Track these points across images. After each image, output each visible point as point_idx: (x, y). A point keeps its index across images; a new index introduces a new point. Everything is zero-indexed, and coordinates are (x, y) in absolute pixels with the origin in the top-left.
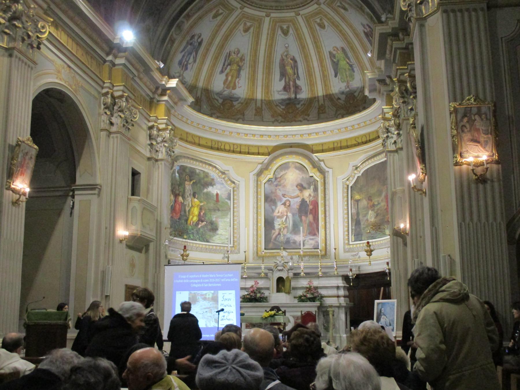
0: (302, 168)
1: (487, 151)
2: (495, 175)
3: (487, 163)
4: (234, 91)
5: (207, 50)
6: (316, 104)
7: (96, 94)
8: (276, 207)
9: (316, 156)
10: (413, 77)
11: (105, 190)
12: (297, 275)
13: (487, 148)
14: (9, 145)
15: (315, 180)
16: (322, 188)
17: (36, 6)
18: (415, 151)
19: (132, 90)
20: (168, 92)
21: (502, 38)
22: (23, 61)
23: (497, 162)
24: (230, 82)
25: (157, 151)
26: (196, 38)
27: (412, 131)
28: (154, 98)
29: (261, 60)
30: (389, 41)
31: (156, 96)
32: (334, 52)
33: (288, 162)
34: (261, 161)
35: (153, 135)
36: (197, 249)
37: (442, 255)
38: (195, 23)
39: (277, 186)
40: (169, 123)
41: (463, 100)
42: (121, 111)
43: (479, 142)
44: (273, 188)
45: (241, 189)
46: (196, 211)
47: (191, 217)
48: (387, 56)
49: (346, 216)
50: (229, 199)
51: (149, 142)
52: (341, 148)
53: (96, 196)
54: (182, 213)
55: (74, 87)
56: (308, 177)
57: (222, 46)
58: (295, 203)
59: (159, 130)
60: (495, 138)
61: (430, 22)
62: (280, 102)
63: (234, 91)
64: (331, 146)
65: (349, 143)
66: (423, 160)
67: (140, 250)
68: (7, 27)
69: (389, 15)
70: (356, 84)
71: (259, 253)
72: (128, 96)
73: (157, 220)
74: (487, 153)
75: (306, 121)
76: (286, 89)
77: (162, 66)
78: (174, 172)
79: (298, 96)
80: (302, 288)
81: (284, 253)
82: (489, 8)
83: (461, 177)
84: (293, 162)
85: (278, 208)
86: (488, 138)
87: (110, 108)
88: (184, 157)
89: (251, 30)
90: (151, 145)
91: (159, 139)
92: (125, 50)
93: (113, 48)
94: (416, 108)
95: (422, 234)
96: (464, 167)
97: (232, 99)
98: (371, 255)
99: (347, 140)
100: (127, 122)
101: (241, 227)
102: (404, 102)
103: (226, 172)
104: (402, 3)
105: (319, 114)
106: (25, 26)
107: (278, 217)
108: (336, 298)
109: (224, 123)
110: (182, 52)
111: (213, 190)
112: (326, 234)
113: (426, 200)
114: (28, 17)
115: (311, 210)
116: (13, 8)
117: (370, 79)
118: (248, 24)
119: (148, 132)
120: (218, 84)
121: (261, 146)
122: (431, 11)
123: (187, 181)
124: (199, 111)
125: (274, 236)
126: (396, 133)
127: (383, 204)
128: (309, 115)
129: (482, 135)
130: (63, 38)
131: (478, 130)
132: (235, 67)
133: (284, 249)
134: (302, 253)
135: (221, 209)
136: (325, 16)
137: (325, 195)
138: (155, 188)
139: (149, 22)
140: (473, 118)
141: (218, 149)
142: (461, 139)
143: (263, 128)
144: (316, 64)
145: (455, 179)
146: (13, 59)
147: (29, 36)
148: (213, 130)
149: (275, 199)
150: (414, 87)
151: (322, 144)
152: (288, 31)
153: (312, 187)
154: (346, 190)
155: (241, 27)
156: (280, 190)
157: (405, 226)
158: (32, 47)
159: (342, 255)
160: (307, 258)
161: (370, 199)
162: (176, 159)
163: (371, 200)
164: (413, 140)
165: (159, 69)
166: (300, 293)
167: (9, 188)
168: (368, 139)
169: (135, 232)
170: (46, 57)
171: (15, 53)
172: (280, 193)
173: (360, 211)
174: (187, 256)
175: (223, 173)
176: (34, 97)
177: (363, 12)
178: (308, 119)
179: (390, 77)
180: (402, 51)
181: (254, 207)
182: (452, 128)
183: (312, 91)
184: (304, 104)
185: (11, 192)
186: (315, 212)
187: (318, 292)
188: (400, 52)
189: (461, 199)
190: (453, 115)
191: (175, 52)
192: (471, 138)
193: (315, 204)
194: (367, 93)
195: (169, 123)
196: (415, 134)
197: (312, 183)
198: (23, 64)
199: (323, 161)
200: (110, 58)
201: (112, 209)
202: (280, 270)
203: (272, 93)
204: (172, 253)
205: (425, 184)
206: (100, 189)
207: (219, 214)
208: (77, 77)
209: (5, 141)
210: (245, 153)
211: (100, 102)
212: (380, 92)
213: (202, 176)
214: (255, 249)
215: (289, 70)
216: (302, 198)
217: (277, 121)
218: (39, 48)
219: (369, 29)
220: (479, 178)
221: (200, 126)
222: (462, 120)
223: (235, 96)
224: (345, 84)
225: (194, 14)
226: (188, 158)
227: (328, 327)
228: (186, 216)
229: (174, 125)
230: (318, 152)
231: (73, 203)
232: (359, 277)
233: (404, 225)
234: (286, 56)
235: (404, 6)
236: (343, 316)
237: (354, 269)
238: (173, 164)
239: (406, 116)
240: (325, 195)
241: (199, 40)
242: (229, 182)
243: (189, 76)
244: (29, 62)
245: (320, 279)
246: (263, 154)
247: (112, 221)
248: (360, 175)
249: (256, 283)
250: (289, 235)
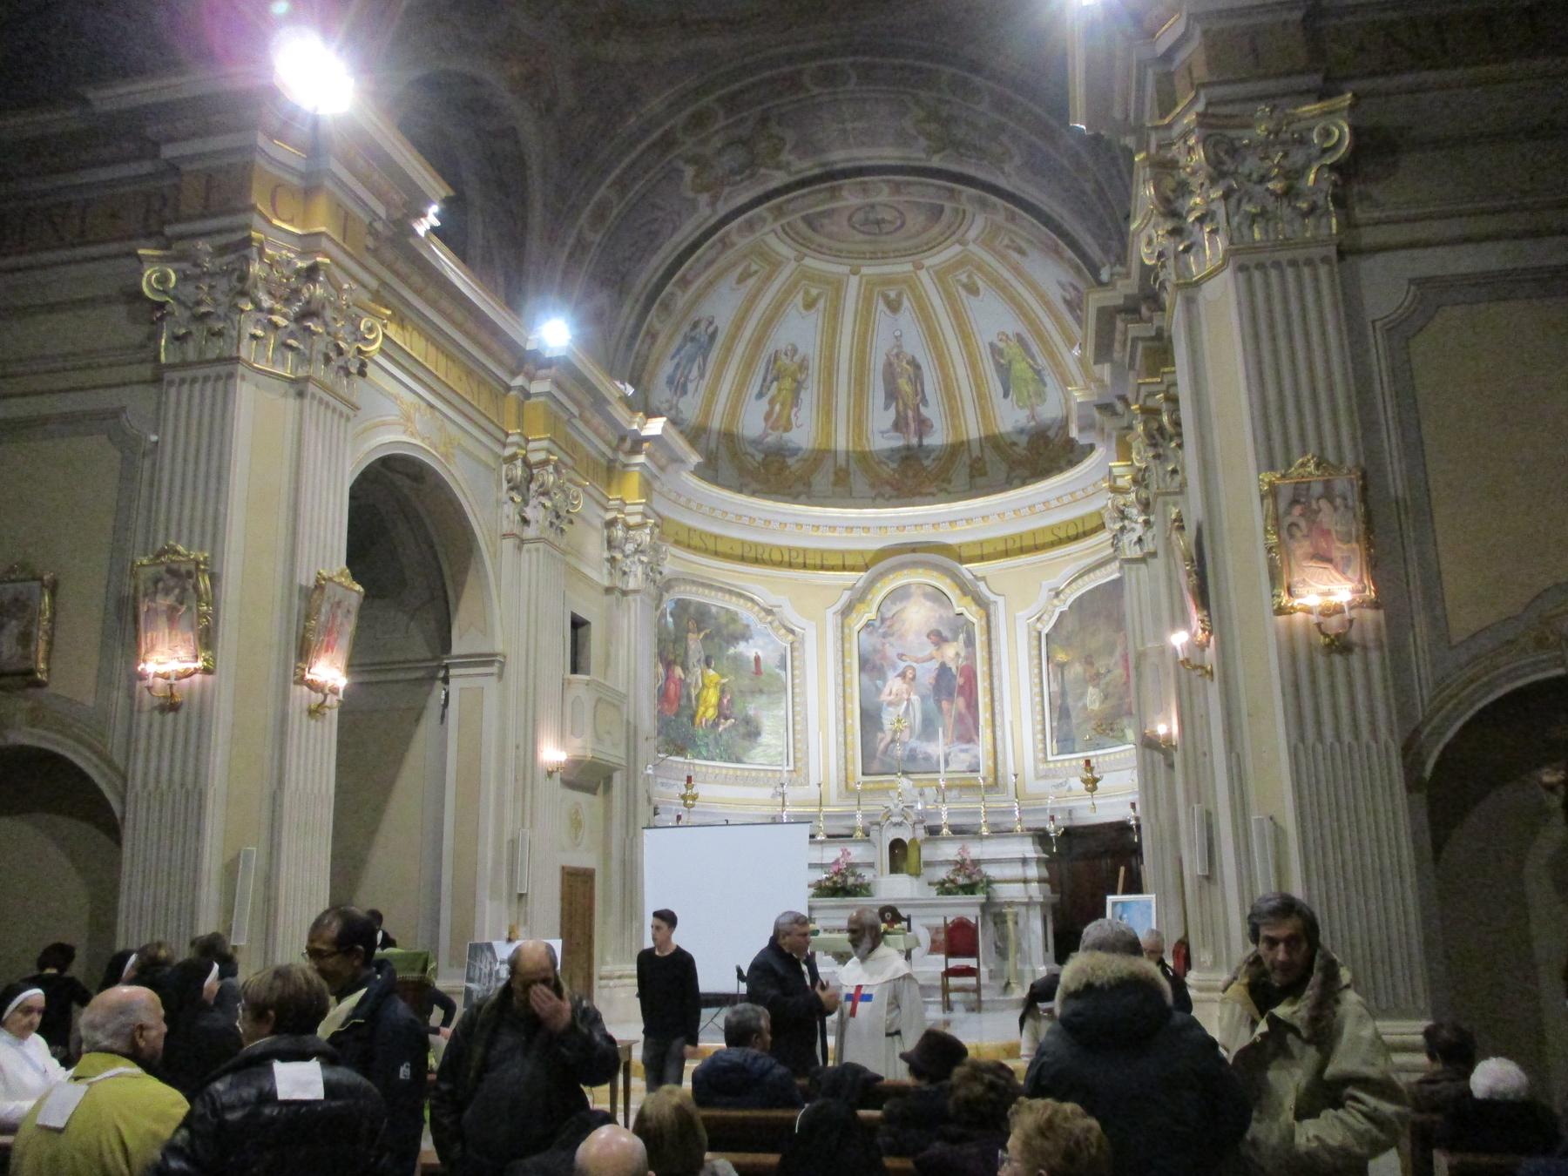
0: (938, 596)
1: (1349, 579)
2: (1371, 635)
3: (1351, 608)
4: (786, 436)
5: (728, 350)
6: (966, 458)
7: (491, 462)
8: (885, 680)
10: (1173, 400)
11: (513, 668)
12: (933, 831)
13: (1350, 574)
14: (301, 588)
15: (968, 622)
16: (984, 638)
17: (354, 286)
18: (1183, 579)
19: (571, 448)
20: (646, 445)
21: (1373, 322)
22: (327, 405)
23: (1376, 605)
24: (780, 415)
25: (625, 573)
26: (703, 326)
27: (1175, 535)
28: (614, 461)
29: (844, 366)
30: (1120, 325)
31: (621, 457)
32: (1001, 345)
33: (909, 585)
34: (850, 583)
36: (717, 780)
37: (1254, 817)
38: (699, 297)
39: (885, 635)
40: (649, 512)
41: (1290, 466)
42: (546, 494)
43: (1330, 561)
44: (875, 640)
45: (807, 646)
46: (712, 696)
47: (702, 709)
48: (1116, 356)
49: (1038, 699)
51: (606, 555)
52: (1023, 551)
53: (494, 679)
54: (684, 702)
55: (442, 449)
56: (951, 615)
57: (758, 342)
58: (927, 673)
59: (628, 527)
60: (1368, 549)
61: (1210, 290)
63: (786, 436)
64: (1001, 547)
65: (1040, 541)
66: (1202, 597)
67: (592, 790)
68: (292, 335)
69: (1118, 269)
70: (1050, 411)
71: (851, 783)
72: (560, 460)
73: (628, 722)
74: (1350, 586)
75: (943, 495)
76: (899, 425)
77: (630, 391)
78: (663, 615)
80: (948, 862)
81: (904, 783)
82: (1342, 254)
83: (1291, 638)
84: (920, 585)
85: (890, 683)
86: (1353, 550)
87: (520, 487)
89: (821, 304)
90: (612, 560)
92: (549, 364)
93: (525, 361)
94: (1183, 469)
95: (1206, 749)
96: (1299, 616)
98: (1094, 788)
99: (1034, 533)
100: (558, 517)
101: (808, 735)
102: (1157, 457)
104: (1144, 250)
105: (972, 477)
106: (331, 330)
107: (890, 704)
108: (1021, 885)
109: (768, 504)
110: (673, 357)
111: (747, 650)
112: (994, 739)
113: (1214, 689)
114: (338, 309)
115: (961, 687)
116: (306, 294)
117: (1081, 404)
118: (814, 292)
120: (753, 422)
121: (850, 552)
122: (1209, 267)
123: (690, 633)
124: (714, 481)
125: (882, 746)
126: (1141, 519)
127: (1119, 671)
128: (949, 482)
129: (1338, 544)
130: (415, 345)
131: (1326, 533)
132: (787, 383)
133: (905, 773)
134: (942, 784)
136: (979, 268)
137: (990, 653)
138: (623, 653)
139: (602, 298)
140: (1314, 506)
141: (757, 561)
142: (1289, 554)
143: (852, 513)
144: (961, 372)
145: (1278, 641)
146: (307, 401)
147: (340, 352)
148: (745, 520)
150: (1177, 424)
151: (981, 543)
152: (900, 303)
153: (962, 637)
154: (1035, 643)
155: (799, 299)
157: (1170, 729)
158: (348, 374)
159: (1033, 786)
160: (955, 793)
161: (1089, 661)
162: (668, 585)
163: (1091, 664)
164: (1178, 555)
165: (625, 400)
166: (942, 873)
167: (301, 681)
168: (1081, 530)
169: (580, 752)
170: (381, 391)
171: (311, 388)
172: (891, 652)
173: (1068, 687)
174: (694, 798)
175: (769, 612)
176: (358, 472)
177: (1062, 257)
179: (1123, 399)
180: (1150, 344)
182: (1266, 531)
183: (955, 427)
184: (938, 459)
185: (306, 689)
186: (969, 691)
187: (980, 871)
188: (1145, 349)
189: (1294, 689)
190: (1269, 501)
191: (658, 360)
192: (1311, 550)
193: (970, 675)
194: (1074, 433)
195: (649, 512)
196: (1183, 542)
197: (960, 626)
198: (329, 413)
199: (983, 579)
200: (519, 381)
201: (530, 713)
202: (895, 825)
204: (663, 789)
205: (1211, 652)
206: (503, 664)
207: (763, 699)
208: (450, 427)
209: (291, 581)
210: (815, 567)
211: (500, 475)
212: (1102, 430)
213: (723, 619)
214: (843, 773)
215: (904, 385)
217: (883, 496)
218: (362, 373)
219: (1073, 293)
220: (1332, 641)
222: (1288, 513)
224: (1027, 412)
225: (698, 275)
226: (694, 582)
227: (1006, 948)
228: (690, 707)
229: (659, 515)
230: (971, 560)
231: (447, 695)
232: (1071, 834)
233: (1166, 726)
234: (897, 356)
235: (1149, 256)
236: (1036, 925)
237: (1058, 817)
238: (660, 599)
240: (990, 653)
241: (711, 329)
242: (783, 631)
243: (690, 407)
244: (340, 406)
245: (986, 842)
246: (853, 569)
247: (530, 730)
249: (846, 853)
250: (914, 743)
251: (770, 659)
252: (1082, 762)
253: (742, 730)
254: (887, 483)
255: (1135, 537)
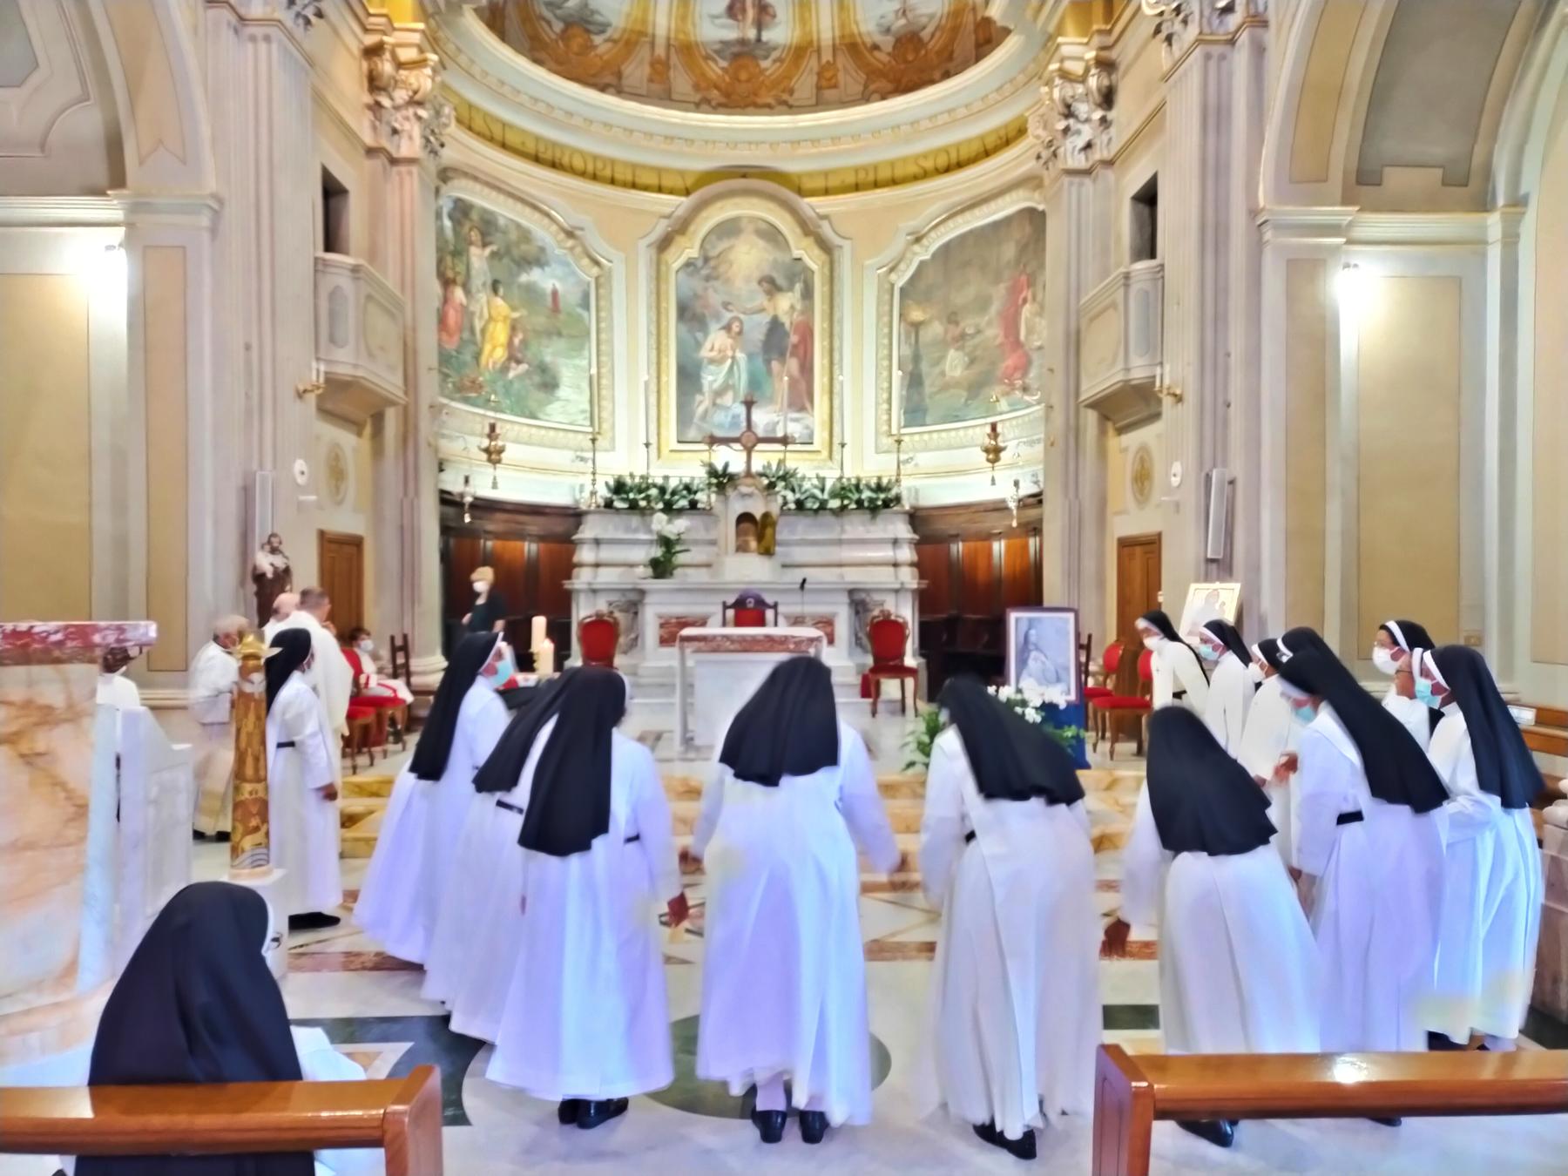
0: (772, 235)
6: (812, 63)
8: (706, 334)
9: (813, 205)
25: (395, 131)
34: (667, 210)
35: (380, 75)
39: (708, 278)
44: (696, 284)
46: (500, 333)
47: (487, 348)
50: (586, 306)
51: (367, 98)
58: (757, 327)
62: (717, 47)
79: (766, 36)
84: (753, 219)
88: (466, 175)
90: (377, 107)
91: (401, 95)
97: (591, 28)
98: (997, 459)
99: (892, 164)
103: (578, 233)
107: (712, 361)
108: (891, 569)
111: (544, 279)
115: (795, 346)
119: (365, 65)
135: (565, 332)
141: (554, 165)
149: (704, 315)
153: (798, 287)
156: (716, 291)
161: (952, 318)
163: (957, 323)
172: (715, 298)
173: (923, 351)
178: (791, 101)
181: (649, 332)
184: (779, 60)
197: (797, 274)
199: (825, 217)
203: (697, 20)
207: (560, 344)
216: (772, 313)
217: (707, 101)
221: (506, 90)
223: (598, 18)
228: (475, 343)
239: (1206, 30)
242: (586, 261)
246: (671, 192)
248: (927, 257)
251: (569, 296)
252: (988, 430)
253: (537, 379)
254: (716, 87)
255: (1081, 142)
